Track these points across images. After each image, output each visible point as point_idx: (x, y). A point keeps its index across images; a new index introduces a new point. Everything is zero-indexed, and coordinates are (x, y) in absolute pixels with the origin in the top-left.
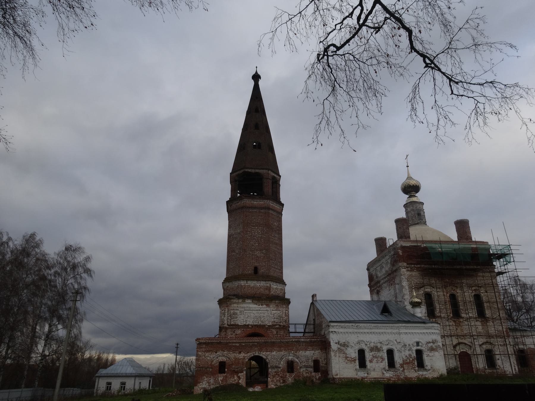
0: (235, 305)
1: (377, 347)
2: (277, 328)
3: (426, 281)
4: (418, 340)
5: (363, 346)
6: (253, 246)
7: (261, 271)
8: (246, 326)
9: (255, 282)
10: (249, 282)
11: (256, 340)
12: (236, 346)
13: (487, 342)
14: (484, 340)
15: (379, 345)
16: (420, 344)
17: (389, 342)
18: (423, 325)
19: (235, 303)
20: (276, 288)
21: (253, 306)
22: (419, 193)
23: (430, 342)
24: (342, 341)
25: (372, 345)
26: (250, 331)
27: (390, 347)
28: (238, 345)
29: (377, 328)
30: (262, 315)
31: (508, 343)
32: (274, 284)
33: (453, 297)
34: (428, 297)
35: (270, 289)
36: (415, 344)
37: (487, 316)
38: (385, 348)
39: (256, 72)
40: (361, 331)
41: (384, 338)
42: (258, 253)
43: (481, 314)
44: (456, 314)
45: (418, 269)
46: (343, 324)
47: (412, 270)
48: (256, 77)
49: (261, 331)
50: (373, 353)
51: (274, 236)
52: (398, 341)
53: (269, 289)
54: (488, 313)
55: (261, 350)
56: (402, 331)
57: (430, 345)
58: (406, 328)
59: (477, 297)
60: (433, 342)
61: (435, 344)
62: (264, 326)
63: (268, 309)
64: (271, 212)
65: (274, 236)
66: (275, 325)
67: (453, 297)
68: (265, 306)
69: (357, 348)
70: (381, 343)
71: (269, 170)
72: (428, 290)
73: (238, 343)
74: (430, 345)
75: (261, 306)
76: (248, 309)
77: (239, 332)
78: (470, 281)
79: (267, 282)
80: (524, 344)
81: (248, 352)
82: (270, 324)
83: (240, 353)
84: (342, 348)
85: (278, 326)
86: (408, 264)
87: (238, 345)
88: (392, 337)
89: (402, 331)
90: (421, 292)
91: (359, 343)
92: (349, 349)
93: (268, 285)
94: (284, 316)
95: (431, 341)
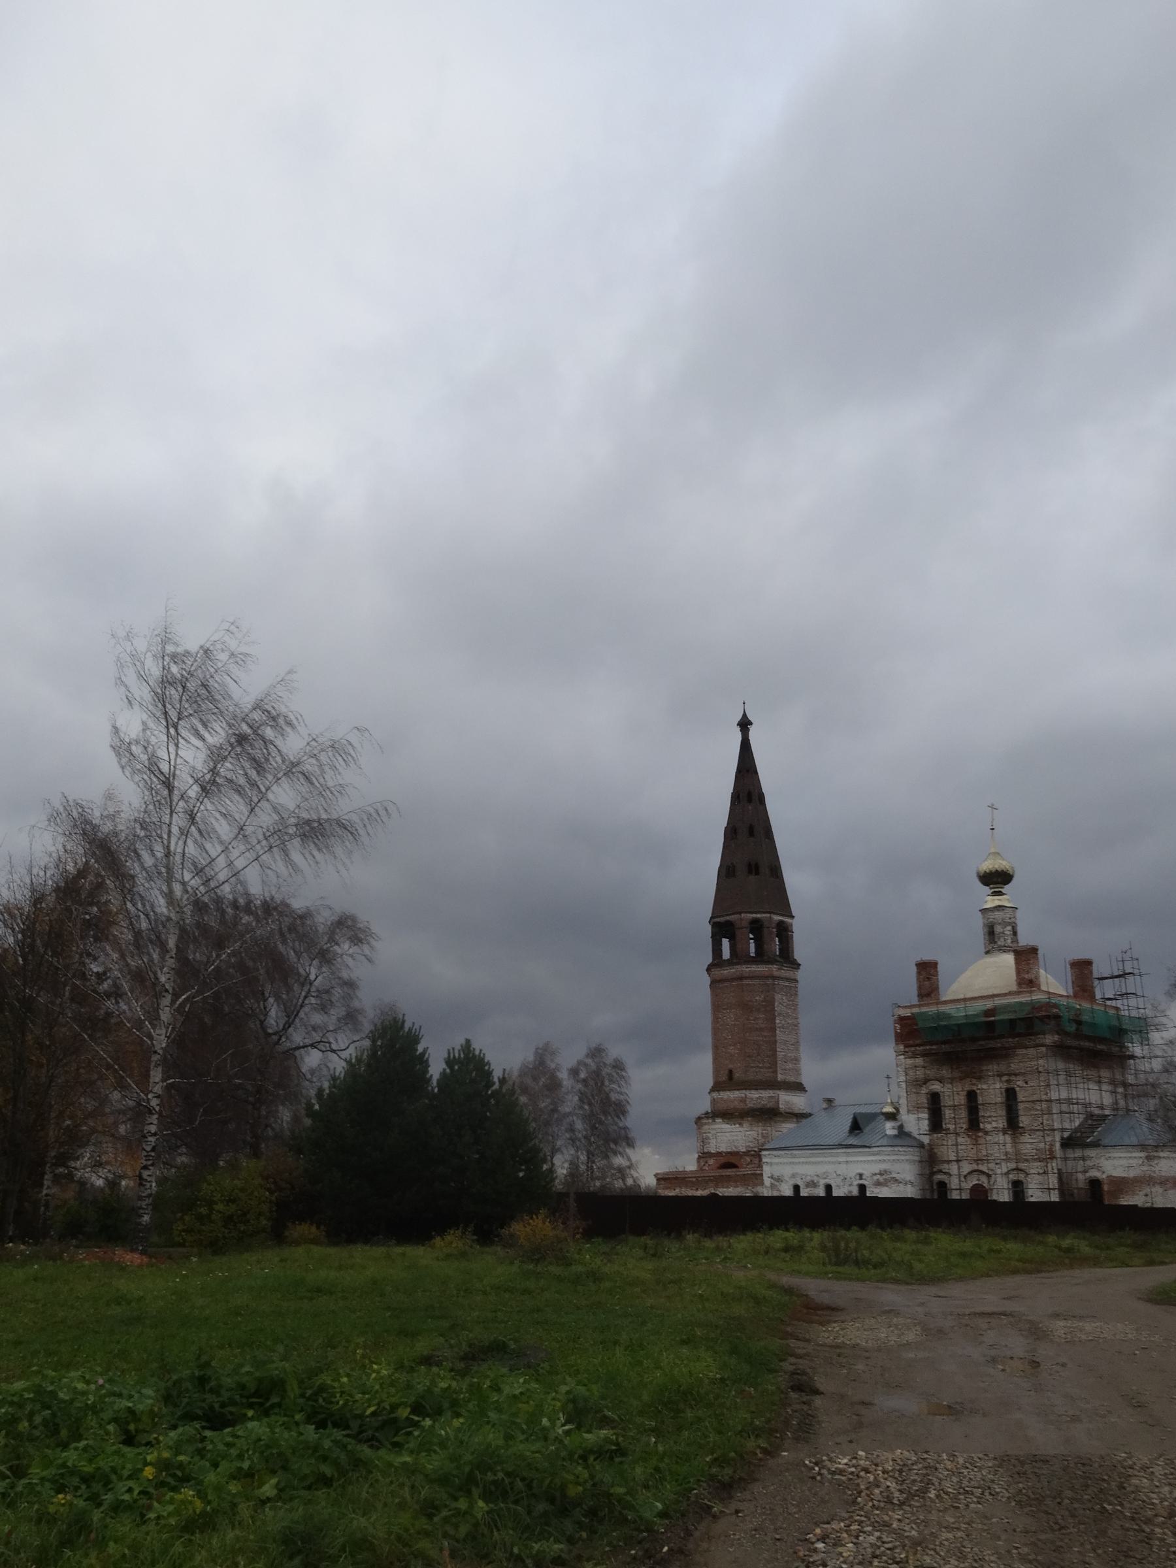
0: (706, 1127)
1: (813, 1181)
2: (752, 1155)
3: (931, 1073)
4: (860, 1171)
5: (800, 1183)
6: (726, 1039)
7: (737, 1075)
8: (719, 1154)
9: (728, 1093)
10: (722, 1093)
11: (729, 1172)
12: (692, 1182)
13: (1017, 1169)
14: (1012, 1165)
15: (816, 1179)
16: (864, 1177)
17: (826, 1175)
18: (867, 1150)
19: (706, 1124)
20: (760, 1098)
21: (726, 1127)
22: (1010, 884)
23: (876, 1174)
24: (776, 1175)
25: (809, 1179)
26: (722, 1160)
27: (827, 1181)
28: (694, 1180)
29: (813, 1156)
30: (735, 1138)
31: (1050, 1169)
32: (753, 1092)
33: (972, 1096)
34: (935, 1098)
35: (745, 1101)
36: (858, 1177)
37: (1021, 1125)
38: (822, 1182)
39: (745, 715)
40: (797, 1160)
41: (820, 1169)
42: (732, 1050)
43: (1013, 1125)
44: (974, 1124)
45: (924, 1055)
46: (775, 1153)
47: (914, 1056)
48: (745, 724)
49: (733, 1160)
50: (809, 1189)
51: (756, 1019)
52: (838, 1173)
53: (743, 1100)
54: (1024, 1121)
55: (717, 1186)
56: (840, 1159)
57: (875, 1178)
58: (848, 1154)
59: (1010, 1095)
60: (881, 1174)
61: (884, 1177)
62: (738, 1152)
63: (741, 1129)
64: (746, 982)
65: (756, 1019)
66: (749, 1151)
67: (972, 1096)
68: (737, 1125)
69: (792, 1182)
70: (818, 1176)
71: (740, 913)
72: (936, 1087)
73: (695, 1177)
74: (875, 1178)
75: (733, 1126)
76: (719, 1130)
77: (711, 1162)
78: (1002, 1067)
79: (741, 1091)
80: (1098, 1168)
81: (705, 1189)
82: (744, 1150)
83: (697, 1189)
84: (776, 1183)
85: (753, 1153)
86: (906, 1046)
87: (694, 1180)
88: (829, 1168)
89: (840, 1159)
90: (924, 1090)
91: (794, 1176)
92: (783, 1184)
93: (743, 1095)
94: (760, 1138)
95: (877, 1172)
